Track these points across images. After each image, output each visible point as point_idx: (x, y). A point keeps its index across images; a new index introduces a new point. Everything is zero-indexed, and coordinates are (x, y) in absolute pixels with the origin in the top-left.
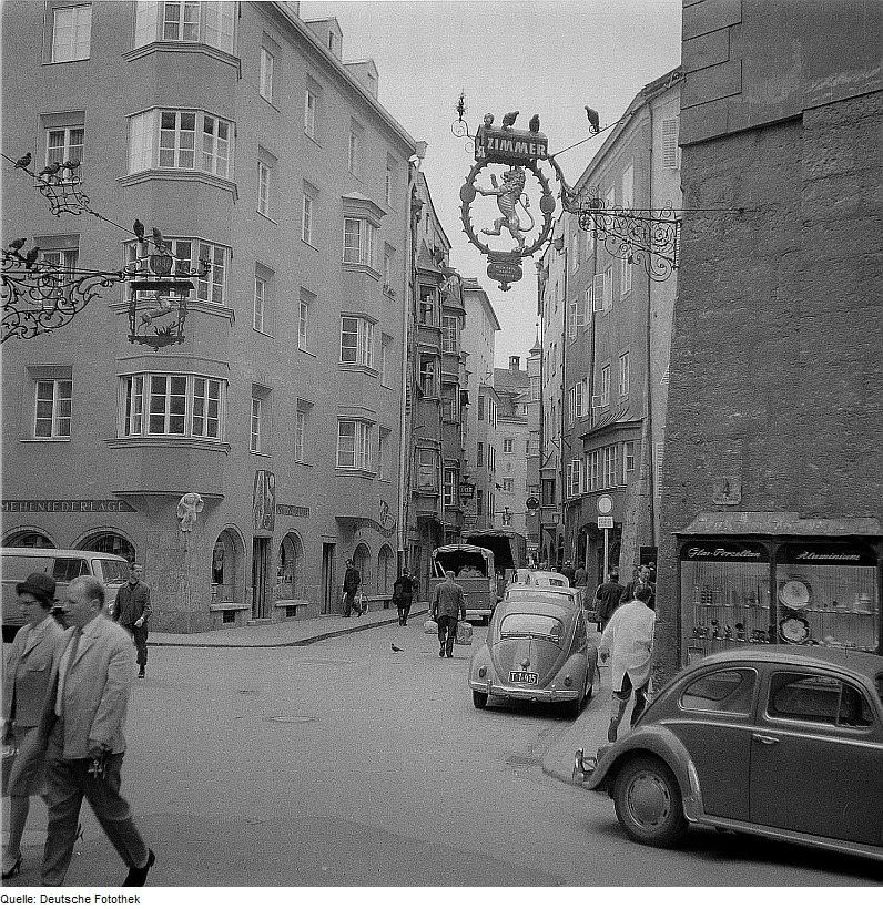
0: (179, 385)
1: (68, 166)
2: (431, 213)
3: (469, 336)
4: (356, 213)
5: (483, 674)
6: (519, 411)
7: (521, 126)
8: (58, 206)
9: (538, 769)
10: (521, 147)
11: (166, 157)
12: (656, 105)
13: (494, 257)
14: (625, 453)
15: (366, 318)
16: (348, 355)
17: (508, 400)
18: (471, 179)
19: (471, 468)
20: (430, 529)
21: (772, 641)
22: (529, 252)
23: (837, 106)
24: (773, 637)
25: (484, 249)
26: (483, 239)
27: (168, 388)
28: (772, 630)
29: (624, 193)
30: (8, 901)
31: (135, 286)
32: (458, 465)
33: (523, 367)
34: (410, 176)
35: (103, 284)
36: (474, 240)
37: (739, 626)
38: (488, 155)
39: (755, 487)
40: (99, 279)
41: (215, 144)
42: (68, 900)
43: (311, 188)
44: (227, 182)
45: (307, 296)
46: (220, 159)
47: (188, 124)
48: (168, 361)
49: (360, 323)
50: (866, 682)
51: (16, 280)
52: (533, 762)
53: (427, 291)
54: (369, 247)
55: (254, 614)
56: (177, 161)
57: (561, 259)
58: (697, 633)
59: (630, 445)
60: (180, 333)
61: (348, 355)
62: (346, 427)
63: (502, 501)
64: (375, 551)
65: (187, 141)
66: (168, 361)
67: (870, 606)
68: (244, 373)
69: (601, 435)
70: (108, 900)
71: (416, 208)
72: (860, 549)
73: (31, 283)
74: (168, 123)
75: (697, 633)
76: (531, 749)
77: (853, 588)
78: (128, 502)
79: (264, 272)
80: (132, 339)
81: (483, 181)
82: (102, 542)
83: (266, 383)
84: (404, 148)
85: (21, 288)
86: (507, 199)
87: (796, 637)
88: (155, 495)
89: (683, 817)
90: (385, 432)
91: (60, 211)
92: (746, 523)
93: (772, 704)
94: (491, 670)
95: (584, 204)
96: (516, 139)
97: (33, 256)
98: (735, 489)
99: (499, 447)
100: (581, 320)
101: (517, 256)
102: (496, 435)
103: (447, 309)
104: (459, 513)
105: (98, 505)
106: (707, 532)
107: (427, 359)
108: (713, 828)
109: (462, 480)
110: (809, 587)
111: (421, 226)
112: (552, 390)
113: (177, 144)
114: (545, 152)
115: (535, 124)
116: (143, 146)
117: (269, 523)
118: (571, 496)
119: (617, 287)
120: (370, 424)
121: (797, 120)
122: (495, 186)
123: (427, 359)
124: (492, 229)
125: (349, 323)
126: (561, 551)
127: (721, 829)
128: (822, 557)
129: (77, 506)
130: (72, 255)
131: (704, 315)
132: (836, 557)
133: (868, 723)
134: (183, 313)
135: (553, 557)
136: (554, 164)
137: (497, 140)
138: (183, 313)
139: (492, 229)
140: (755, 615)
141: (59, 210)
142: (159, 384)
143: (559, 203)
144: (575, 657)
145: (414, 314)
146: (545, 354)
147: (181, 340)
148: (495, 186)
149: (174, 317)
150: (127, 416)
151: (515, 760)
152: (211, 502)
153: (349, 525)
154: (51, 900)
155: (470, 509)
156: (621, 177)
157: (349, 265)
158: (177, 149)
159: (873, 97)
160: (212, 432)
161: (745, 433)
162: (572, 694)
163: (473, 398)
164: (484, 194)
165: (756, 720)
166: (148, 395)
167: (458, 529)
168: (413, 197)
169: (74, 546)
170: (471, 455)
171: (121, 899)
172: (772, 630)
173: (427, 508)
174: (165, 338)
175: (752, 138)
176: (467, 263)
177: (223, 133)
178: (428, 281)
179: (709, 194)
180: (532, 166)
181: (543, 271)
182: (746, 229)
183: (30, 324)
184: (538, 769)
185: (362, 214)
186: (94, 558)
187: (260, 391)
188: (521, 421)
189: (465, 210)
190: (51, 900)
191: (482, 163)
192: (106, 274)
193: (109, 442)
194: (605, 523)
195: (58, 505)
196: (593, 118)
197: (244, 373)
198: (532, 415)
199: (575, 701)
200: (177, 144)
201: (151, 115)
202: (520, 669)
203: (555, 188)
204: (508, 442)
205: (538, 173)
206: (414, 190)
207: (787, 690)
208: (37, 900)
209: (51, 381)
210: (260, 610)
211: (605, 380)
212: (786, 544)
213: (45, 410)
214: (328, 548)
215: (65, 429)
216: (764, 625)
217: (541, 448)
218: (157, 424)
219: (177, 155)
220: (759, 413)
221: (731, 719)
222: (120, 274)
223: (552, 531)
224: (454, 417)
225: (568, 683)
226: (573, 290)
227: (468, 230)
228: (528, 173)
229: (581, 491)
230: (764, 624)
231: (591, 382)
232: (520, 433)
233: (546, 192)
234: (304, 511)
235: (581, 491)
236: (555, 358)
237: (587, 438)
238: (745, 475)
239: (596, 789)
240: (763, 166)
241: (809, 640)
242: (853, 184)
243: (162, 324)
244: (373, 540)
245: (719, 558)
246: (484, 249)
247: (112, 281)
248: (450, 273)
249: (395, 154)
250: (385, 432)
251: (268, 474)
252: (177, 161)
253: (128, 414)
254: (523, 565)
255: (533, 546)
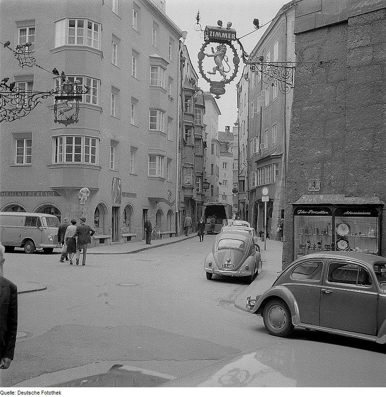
0: (78, 141)
1: (27, 45)
2: (189, 63)
3: (207, 118)
4: (155, 63)
5: (210, 265)
6: (229, 151)
7: (225, 26)
8: (23, 63)
9: (232, 305)
10: (224, 35)
11: (71, 40)
12: (288, 14)
13: (213, 84)
14: (275, 169)
15: (161, 110)
16: (153, 127)
17: (224, 145)
18: (203, 49)
19: (208, 176)
20: (190, 201)
21: (333, 250)
22: (228, 82)
23: (363, 16)
24: (333, 248)
25: (208, 80)
26: (208, 76)
27: (73, 143)
28: (333, 245)
29: (274, 55)
30: (3, 393)
31: (57, 98)
32: (202, 174)
33: (231, 131)
34: (180, 47)
35: (43, 97)
36: (204, 76)
37: (319, 243)
38: (210, 39)
39: (326, 184)
40: (41, 95)
41: (93, 33)
42: (30, 393)
43: (136, 53)
44: (97, 50)
45: (134, 100)
46: (95, 40)
47: (80, 25)
48: (72, 130)
49: (158, 112)
50: (369, 267)
51: (5, 96)
52: (231, 302)
53: (187, 98)
54: (162, 78)
55: (113, 240)
56: (76, 41)
57: (247, 83)
58: (301, 246)
59: (277, 165)
60: (76, 119)
61: (153, 127)
62: (152, 158)
63: (222, 190)
64: (165, 212)
65: (80, 33)
66: (72, 130)
67: (375, 234)
68: (107, 135)
69: (264, 161)
70: (47, 393)
71: (182, 61)
72: (372, 210)
73: (13, 97)
74: (72, 25)
75: (301, 246)
76: (230, 297)
77: (368, 227)
78: (57, 192)
79: (115, 90)
80: (56, 121)
81: (208, 50)
82: (47, 209)
83: (117, 139)
84: (177, 34)
85: (7, 100)
86: (218, 58)
87: (343, 248)
88: (68, 189)
89: (293, 325)
90: (169, 160)
91: (23, 65)
92: (322, 199)
93: (331, 275)
94: (214, 264)
95: (256, 61)
96: (222, 32)
97: (13, 85)
98: (318, 185)
99: (221, 166)
100: (255, 110)
101: (223, 84)
102: (219, 161)
103: (196, 106)
104: (203, 195)
105: (44, 193)
106: (305, 203)
107: (188, 128)
108: (304, 329)
109: (204, 181)
110: (349, 226)
111: (185, 69)
112: (244, 141)
113: (76, 34)
114: (235, 37)
115: (230, 25)
116: (61, 35)
117: (119, 201)
118: (252, 187)
119: (271, 96)
120: (163, 157)
121: (346, 22)
122: (213, 52)
123: (188, 128)
124: (212, 71)
125: (153, 112)
126: (247, 212)
127: (308, 329)
128: (355, 213)
129: (35, 194)
130: (30, 84)
131: (305, 109)
132: (359, 213)
133: (370, 284)
134: (78, 109)
135: (243, 215)
136: (239, 43)
137: (214, 32)
138: (78, 109)
139: (212, 71)
140: (326, 239)
141: (22, 65)
142: (69, 140)
143: (241, 60)
144: (250, 257)
145: (182, 108)
146: (240, 126)
147: (77, 121)
148: (213, 52)
149: (74, 110)
150: (57, 154)
151: (223, 301)
152: (93, 192)
153: (154, 201)
154: (22, 393)
155: (208, 193)
156: (273, 47)
157: (154, 88)
158: (76, 36)
159: (379, 12)
160: (93, 161)
161: (323, 160)
162: (249, 273)
163: (209, 145)
164: (208, 56)
165: (323, 283)
166: (65, 145)
167: (203, 202)
168: (181, 56)
169: (34, 211)
170: (208, 170)
171: (53, 393)
172: (333, 245)
173: (188, 193)
174: (70, 121)
175: (326, 30)
176: (204, 86)
177: (96, 29)
178: (188, 93)
179: (308, 54)
180: (229, 44)
181: (239, 87)
182: (323, 70)
183: (11, 115)
184: (232, 305)
185: (159, 64)
186: (43, 216)
187: (114, 143)
188: (230, 155)
189: (200, 63)
190: (22, 393)
191: (207, 42)
192: (44, 93)
193: (48, 166)
194: (265, 199)
195: (27, 194)
196: (256, 22)
197: (107, 135)
198: (235, 152)
199: (251, 276)
200: (76, 34)
201: (64, 21)
202: (226, 263)
203: (240, 53)
204: (225, 164)
205: (232, 47)
206: (182, 53)
207: (337, 271)
208: (16, 393)
209: (23, 140)
210: (115, 238)
211: (266, 136)
212: (339, 208)
213: (20, 152)
214: (145, 211)
215: (29, 160)
216: (330, 243)
217: (239, 166)
218: (69, 158)
219: (76, 38)
220: (328, 151)
221: (312, 283)
222: (50, 93)
223: (243, 203)
224: (200, 154)
225: (247, 269)
226: (252, 97)
227: (202, 72)
228: (228, 46)
229: (256, 185)
230: (329, 242)
231: (260, 137)
232: (230, 160)
233: (236, 55)
234: (134, 195)
235: (256, 185)
236: (244, 127)
237: (258, 162)
238: (322, 178)
239: (256, 313)
240: (332, 41)
241: (349, 249)
242: (370, 50)
243: (68, 114)
244: (164, 207)
245: (310, 214)
246: (208, 80)
247: (46, 96)
248: (198, 90)
249: (173, 37)
250: (169, 160)
251: (118, 179)
252: (76, 41)
253: (56, 153)
254: (231, 218)
255: (235, 209)
